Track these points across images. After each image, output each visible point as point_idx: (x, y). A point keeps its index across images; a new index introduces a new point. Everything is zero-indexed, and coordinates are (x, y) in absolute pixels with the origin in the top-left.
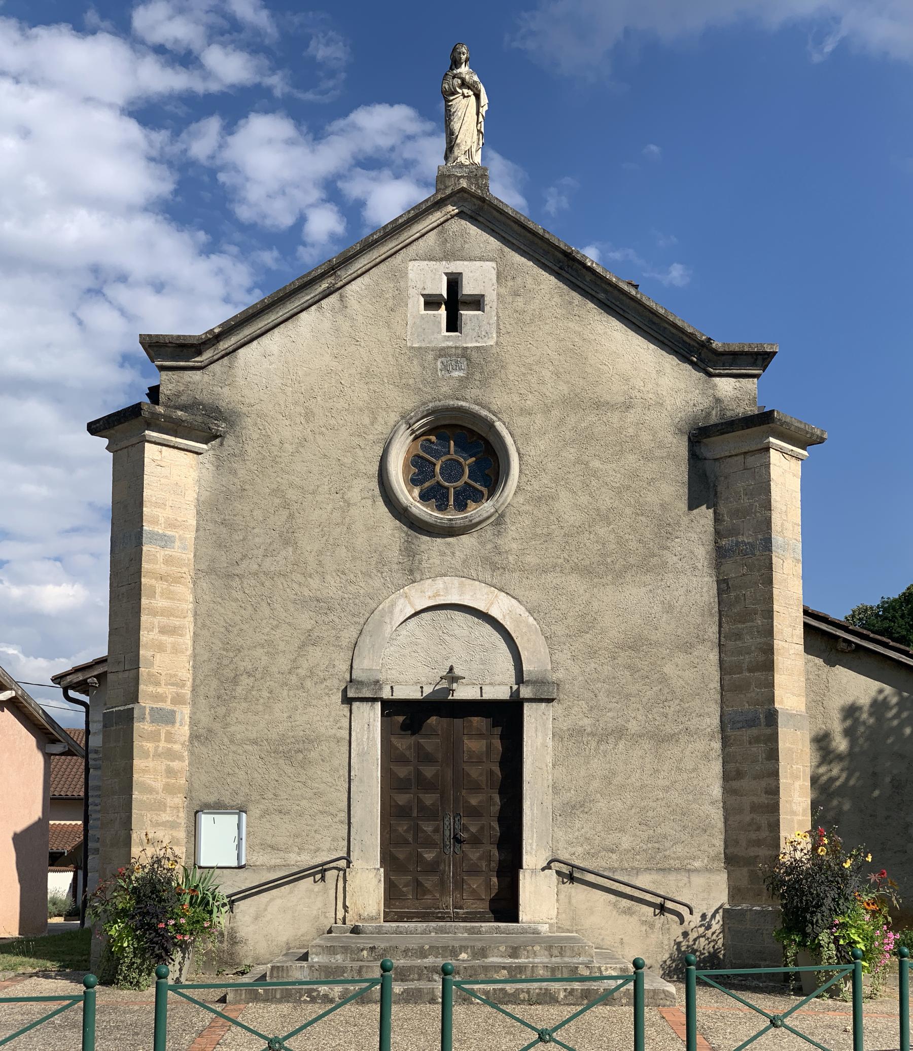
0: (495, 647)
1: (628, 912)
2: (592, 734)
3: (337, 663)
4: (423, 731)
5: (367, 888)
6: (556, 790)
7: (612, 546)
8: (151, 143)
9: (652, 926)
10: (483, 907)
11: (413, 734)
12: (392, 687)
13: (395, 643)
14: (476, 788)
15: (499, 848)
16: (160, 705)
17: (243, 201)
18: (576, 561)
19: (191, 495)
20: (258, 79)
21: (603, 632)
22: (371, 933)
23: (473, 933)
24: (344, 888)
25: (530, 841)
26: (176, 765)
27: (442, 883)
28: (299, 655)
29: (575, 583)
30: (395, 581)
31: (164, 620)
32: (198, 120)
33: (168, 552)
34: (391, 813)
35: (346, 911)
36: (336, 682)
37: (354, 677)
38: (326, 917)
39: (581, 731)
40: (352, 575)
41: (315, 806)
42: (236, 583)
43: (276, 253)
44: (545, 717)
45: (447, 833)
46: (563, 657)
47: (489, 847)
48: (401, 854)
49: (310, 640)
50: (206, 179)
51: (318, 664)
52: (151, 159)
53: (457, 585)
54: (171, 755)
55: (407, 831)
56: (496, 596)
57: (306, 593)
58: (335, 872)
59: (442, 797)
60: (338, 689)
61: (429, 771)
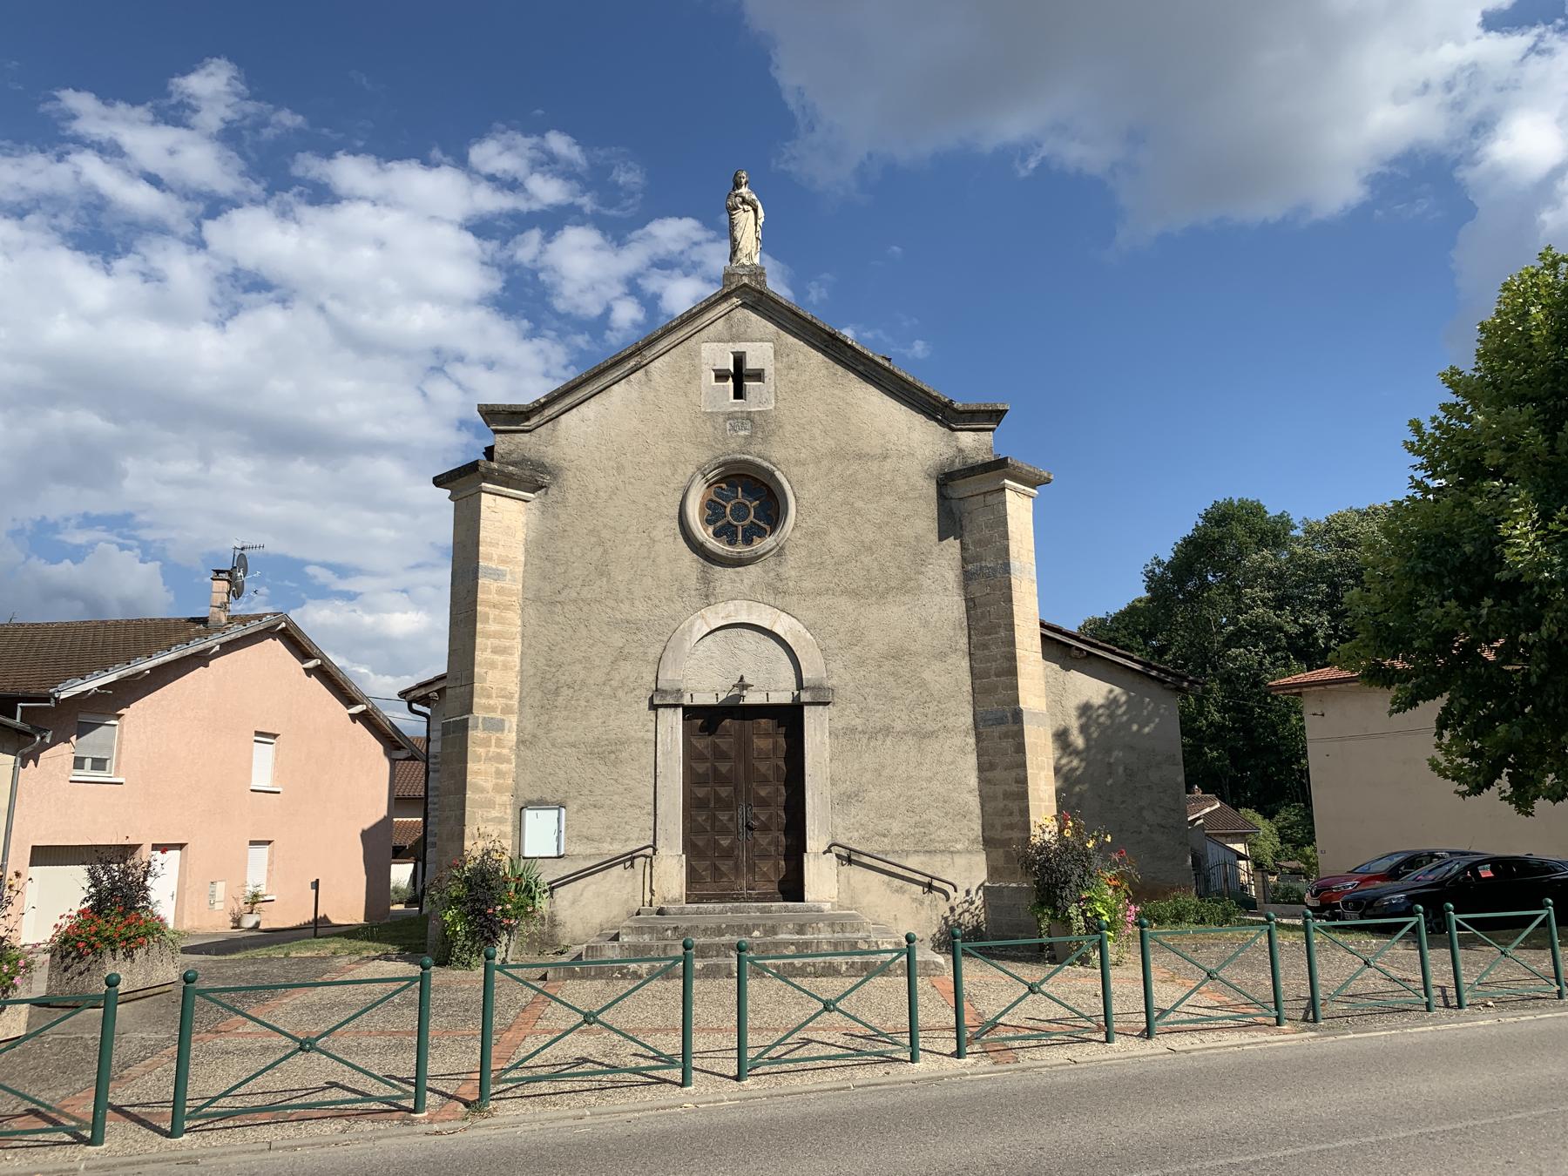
0: (779, 659)
1: (900, 890)
6: (833, 782)
7: (875, 572)
8: (483, 251)
9: (921, 903)
10: (772, 888)
14: (764, 781)
16: (492, 715)
17: (560, 295)
19: (520, 536)
20: (571, 200)
26: (504, 767)
27: (737, 868)
29: (845, 604)
31: (496, 642)
32: (522, 232)
33: (500, 584)
34: (692, 805)
36: (644, 692)
39: (854, 730)
42: (558, 609)
43: (587, 337)
49: (621, 656)
50: (529, 277)
52: (484, 263)
54: (499, 758)
61: (724, 767)
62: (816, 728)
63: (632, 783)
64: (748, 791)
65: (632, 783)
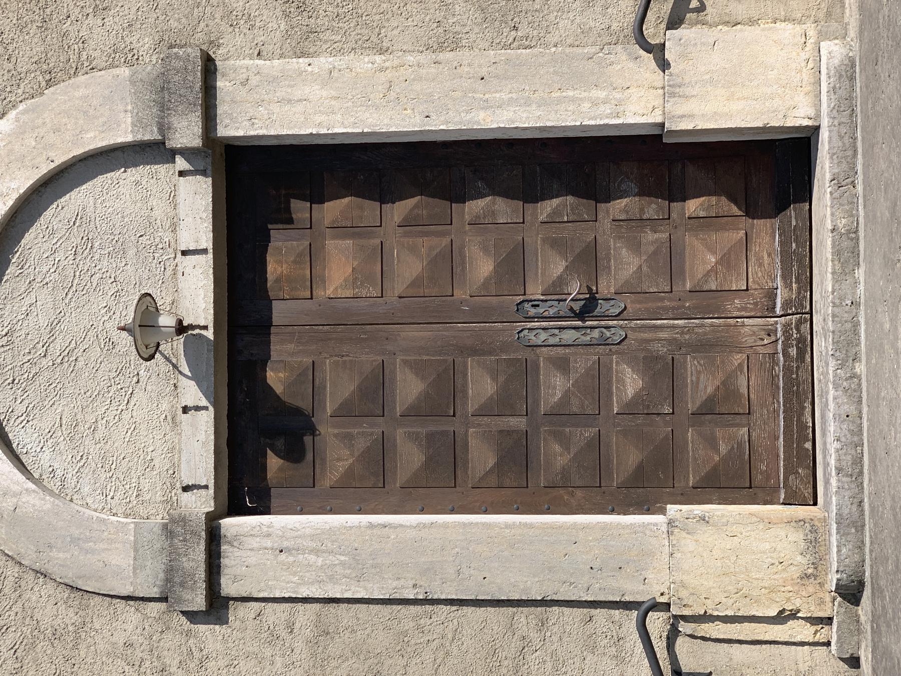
4: (304, 404)
5: (724, 552)
6: (449, 42)
10: (767, 235)
11: (312, 430)
12: (186, 489)
13: (71, 482)
14: (449, 264)
22: (861, 547)
24: (727, 620)
25: (586, 105)
27: (705, 346)
34: (520, 481)
35: (794, 615)
36: (171, 640)
37: (155, 592)
45: (569, 336)
46: (99, 35)
47: (605, 224)
48: (627, 458)
55: (565, 442)
58: (682, 645)
59: (474, 352)
60: (188, 633)
61: (409, 388)
62: (292, 98)
64: (483, 315)
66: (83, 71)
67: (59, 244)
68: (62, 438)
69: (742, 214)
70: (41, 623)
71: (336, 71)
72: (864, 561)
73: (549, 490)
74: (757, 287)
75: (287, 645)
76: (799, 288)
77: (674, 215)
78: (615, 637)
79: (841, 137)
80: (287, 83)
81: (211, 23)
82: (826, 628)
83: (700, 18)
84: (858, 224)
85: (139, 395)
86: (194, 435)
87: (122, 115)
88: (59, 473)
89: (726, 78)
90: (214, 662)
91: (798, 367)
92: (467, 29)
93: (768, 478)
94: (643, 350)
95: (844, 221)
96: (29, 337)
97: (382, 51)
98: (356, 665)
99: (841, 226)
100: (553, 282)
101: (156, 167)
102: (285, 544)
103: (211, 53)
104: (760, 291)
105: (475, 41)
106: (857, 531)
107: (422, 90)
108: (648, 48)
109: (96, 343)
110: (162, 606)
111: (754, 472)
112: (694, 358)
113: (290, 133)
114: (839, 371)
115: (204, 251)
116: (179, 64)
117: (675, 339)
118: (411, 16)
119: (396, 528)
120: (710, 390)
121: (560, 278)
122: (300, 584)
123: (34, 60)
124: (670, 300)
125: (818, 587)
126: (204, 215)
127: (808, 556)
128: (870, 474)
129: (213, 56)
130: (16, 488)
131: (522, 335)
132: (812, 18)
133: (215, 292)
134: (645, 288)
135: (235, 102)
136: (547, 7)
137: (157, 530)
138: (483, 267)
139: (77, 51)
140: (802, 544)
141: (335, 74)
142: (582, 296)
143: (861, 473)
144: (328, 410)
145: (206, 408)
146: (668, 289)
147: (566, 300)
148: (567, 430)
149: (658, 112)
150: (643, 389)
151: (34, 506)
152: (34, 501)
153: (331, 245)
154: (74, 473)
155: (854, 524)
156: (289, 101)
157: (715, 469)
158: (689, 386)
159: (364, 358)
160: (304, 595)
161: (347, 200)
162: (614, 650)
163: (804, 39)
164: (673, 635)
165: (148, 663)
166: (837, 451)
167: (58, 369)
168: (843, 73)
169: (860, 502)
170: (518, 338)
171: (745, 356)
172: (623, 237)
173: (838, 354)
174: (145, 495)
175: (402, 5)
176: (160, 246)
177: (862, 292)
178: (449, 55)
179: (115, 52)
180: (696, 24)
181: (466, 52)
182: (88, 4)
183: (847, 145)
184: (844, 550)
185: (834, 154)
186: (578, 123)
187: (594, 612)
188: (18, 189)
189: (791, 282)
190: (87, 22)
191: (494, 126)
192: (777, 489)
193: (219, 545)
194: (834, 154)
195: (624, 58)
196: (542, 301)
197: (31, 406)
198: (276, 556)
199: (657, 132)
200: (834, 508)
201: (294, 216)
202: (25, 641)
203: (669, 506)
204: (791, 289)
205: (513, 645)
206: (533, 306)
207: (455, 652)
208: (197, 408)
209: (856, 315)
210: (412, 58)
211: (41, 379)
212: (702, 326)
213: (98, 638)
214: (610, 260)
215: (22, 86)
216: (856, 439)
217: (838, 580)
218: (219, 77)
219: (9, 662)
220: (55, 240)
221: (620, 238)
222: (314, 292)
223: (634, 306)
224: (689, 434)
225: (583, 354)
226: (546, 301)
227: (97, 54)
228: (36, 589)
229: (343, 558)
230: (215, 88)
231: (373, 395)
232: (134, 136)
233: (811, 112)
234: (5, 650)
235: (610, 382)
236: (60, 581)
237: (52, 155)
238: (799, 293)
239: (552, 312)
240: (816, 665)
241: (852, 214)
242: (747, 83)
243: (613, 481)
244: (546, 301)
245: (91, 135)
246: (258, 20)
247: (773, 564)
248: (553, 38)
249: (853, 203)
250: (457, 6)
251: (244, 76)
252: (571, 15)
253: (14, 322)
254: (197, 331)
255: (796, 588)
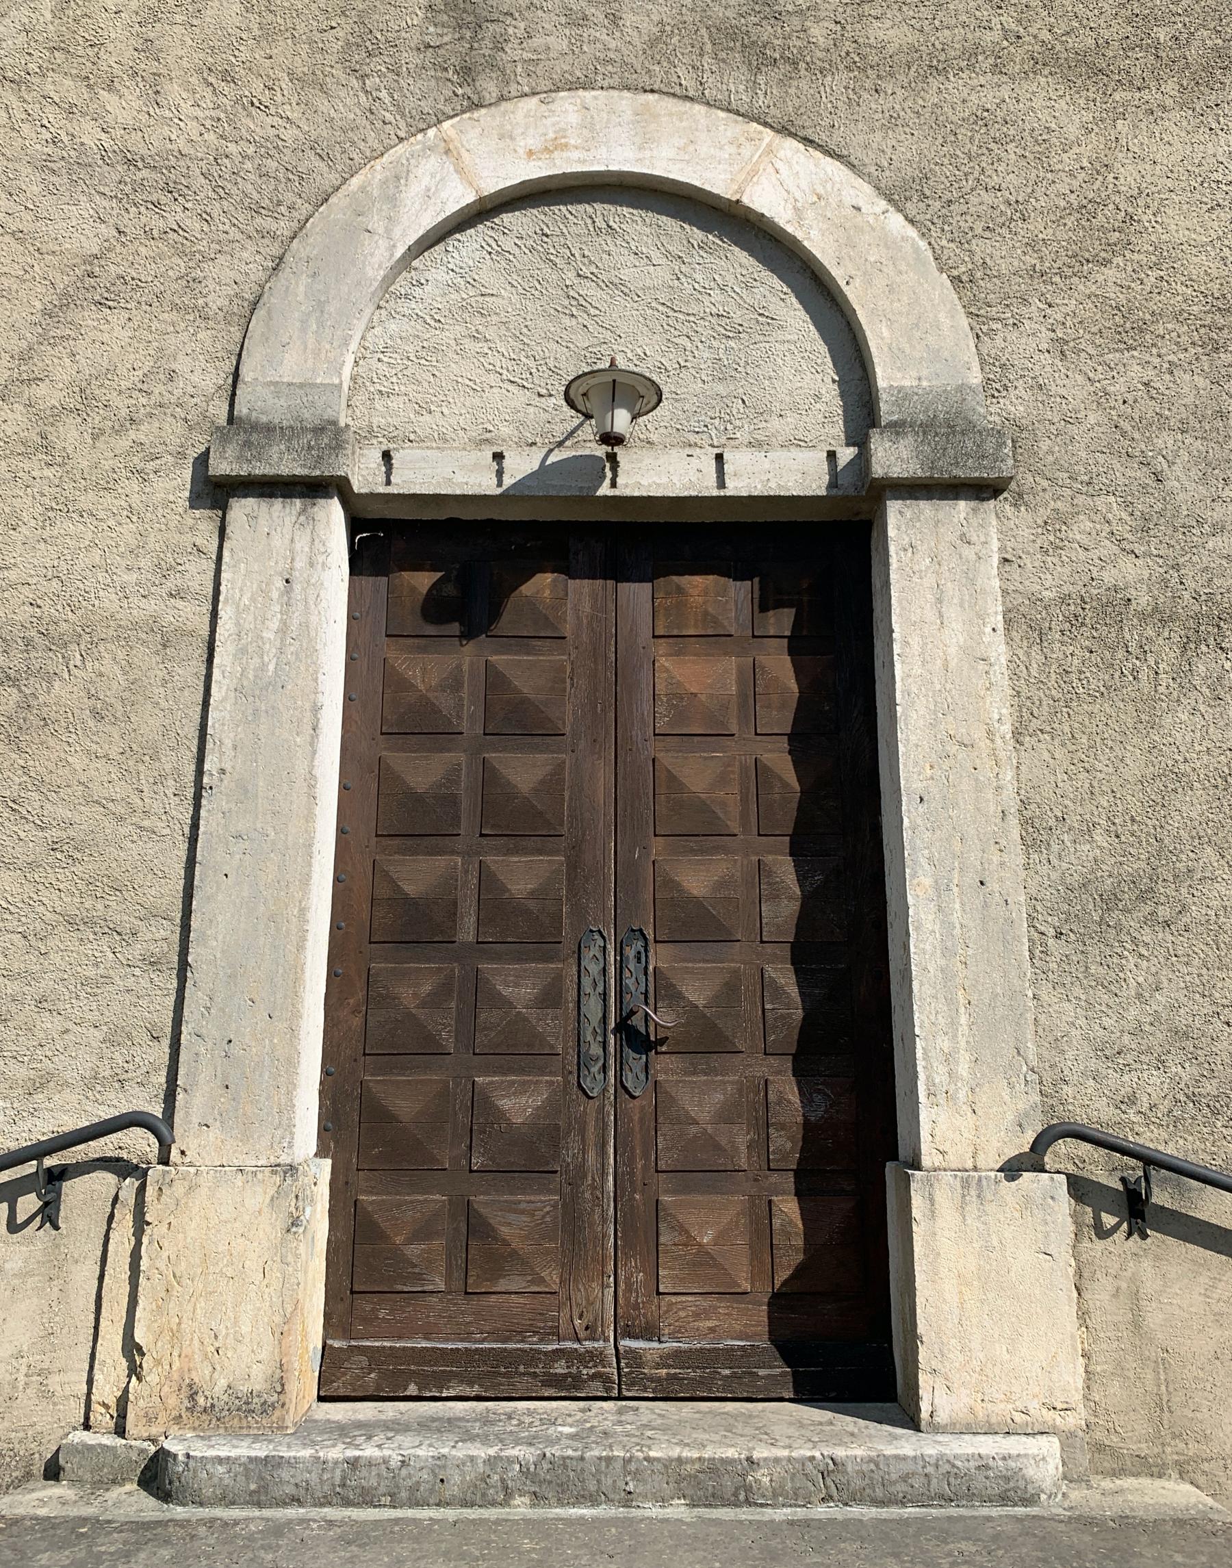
0: (767, 320)
2: (1161, 617)
3: (182, 365)
4: (505, 624)
5: (245, 1251)
6: (1035, 835)
10: (743, 1327)
11: (468, 635)
12: (387, 456)
13: (405, 307)
14: (701, 831)
15: (802, 1070)
18: (1045, 35)
21: (1162, 257)
22: (226, 1500)
23: (715, 1499)
24: (136, 1256)
25: (945, 1044)
27: (572, 1225)
28: (43, 338)
29: (1051, 107)
30: (410, 104)
34: (379, 932)
35: (134, 1370)
36: (173, 432)
37: (241, 409)
38: (46, 1395)
39: (1114, 606)
40: (257, 86)
41: (45, 895)
44: (969, 553)
45: (593, 1008)
46: (1026, 344)
47: (762, 1068)
48: (406, 1096)
51: (111, 371)
53: (628, 115)
55: (434, 1001)
56: (769, 151)
57: (90, 135)
58: (104, 1181)
59: (573, 866)
60: (182, 455)
61: (523, 771)
62: (945, 606)
63: (86, 817)
65: (86, 817)
66: (974, 324)
67: (733, 295)
68: (465, 296)
69: (777, 1287)
70: (210, 263)
71: (987, 668)
72: (201, 1504)
73: (364, 976)
74: (664, 1309)
75: (153, 589)
76: (659, 1380)
77: (774, 1178)
78: (125, 1076)
79: (905, 1478)
80: (967, 597)
81: (1048, 496)
82: (112, 1424)
83: (1085, 1230)
84: (762, 1505)
85: (521, 397)
86: (462, 468)
87: (915, 374)
88: (418, 292)
89: (993, 1274)
90: (137, 489)
91: (535, 1375)
92: (1055, 861)
93: (365, 1320)
94: (570, 1124)
95: (766, 1480)
96: (604, 256)
97: (1017, 735)
98: (115, 685)
99: (758, 1475)
100: (674, 986)
101: (841, 422)
102: (297, 587)
103: (1005, 495)
104: (656, 1315)
105: (1037, 873)
106: (252, 1493)
107: (962, 791)
108: (1042, 1143)
109: (596, 341)
110: (222, 420)
111: (375, 1298)
112: (555, 1206)
113: (893, 601)
114: (517, 1467)
115: (721, 484)
116: (990, 446)
117: (585, 1176)
118: (1071, 779)
119: (312, 744)
120: (504, 1230)
121: (680, 996)
122: (238, 607)
123: (988, 260)
124: (645, 1168)
125: (175, 1413)
126: (773, 484)
127: (225, 1398)
128: (342, 1523)
129: (1001, 498)
130: (397, 232)
131: (597, 936)
132: (1092, 1420)
133: (664, 497)
134: (664, 1129)
135: (936, 526)
136: (1094, 984)
137: (329, 414)
138: (698, 879)
139: (1003, 316)
140: (244, 1388)
141: (982, 666)
142: (652, 1029)
143: (347, 1503)
144: (495, 657)
145: (500, 484)
146: (662, 1165)
147: (647, 1004)
148: (453, 1005)
149: (937, 1160)
150: (510, 1124)
151: (372, 255)
152: (379, 255)
153: (730, 664)
154: (417, 311)
155: (264, 1488)
156: (940, 601)
157: (382, 1236)
158: (512, 1198)
159: (569, 707)
160: (221, 613)
161: (793, 685)
162: (106, 1074)
163: (1059, 1406)
164: (120, 1167)
165: (144, 401)
166: (386, 1461)
167: (560, 292)
168: (1012, 1484)
169: (298, 1500)
170: (592, 931)
171: (555, 1288)
172: (741, 1096)
173: (546, 1466)
174: (381, 402)
175: (1087, 765)
176: (729, 427)
177: (647, 1513)
178: (1015, 833)
179: (1002, 366)
180: (1075, 1223)
181: (1021, 860)
182: (1069, 331)
183: (892, 1489)
184: (221, 1469)
185: (877, 1465)
186: (917, 1031)
187: (166, 1042)
188: (808, 239)
189: (669, 1367)
190: (1043, 329)
191: (910, 900)
192: (348, 1334)
193: (302, 496)
194: (877, 1465)
195: (1021, 1106)
196: (646, 968)
197: (511, 257)
198: (281, 574)
199: (903, 1152)
200: (292, 1454)
201: (771, 613)
202: (188, 244)
203: (329, 1162)
204: (658, 1366)
205: (126, 918)
206: (639, 953)
207: (123, 831)
208: (500, 473)
209: (609, 1500)
210: (1009, 778)
211: (547, 269)
212: (604, 1220)
213: (184, 336)
214: (706, 1074)
215: (951, 245)
216: (404, 1494)
217: (175, 1456)
218: (973, 504)
219: (161, 223)
220: (737, 290)
221: (740, 1091)
222: (662, 640)
223: (637, 1111)
224: (437, 1197)
225: (565, 1029)
226: (646, 974)
227: (999, 342)
228: (258, 257)
229: (271, 667)
230: (956, 498)
231: (515, 721)
232: (884, 389)
233: (942, 1418)
234: (177, 218)
235: (522, 1071)
236: (267, 288)
237: (857, 282)
238: (651, 1379)
239: (630, 982)
240: (55, 1404)
241: (778, 1496)
242: (986, 1308)
243: (372, 1075)
244: (646, 974)
245: (886, 333)
246: (1056, 560)
247: (216, 1337)
248: (1045, 991)
249: (798, 1498)
250: (1088, 846)
251: (974, 539)
252: (1082, 1022)
253: (626, 237)
254: (609, 474)
255: (176, 1376)
